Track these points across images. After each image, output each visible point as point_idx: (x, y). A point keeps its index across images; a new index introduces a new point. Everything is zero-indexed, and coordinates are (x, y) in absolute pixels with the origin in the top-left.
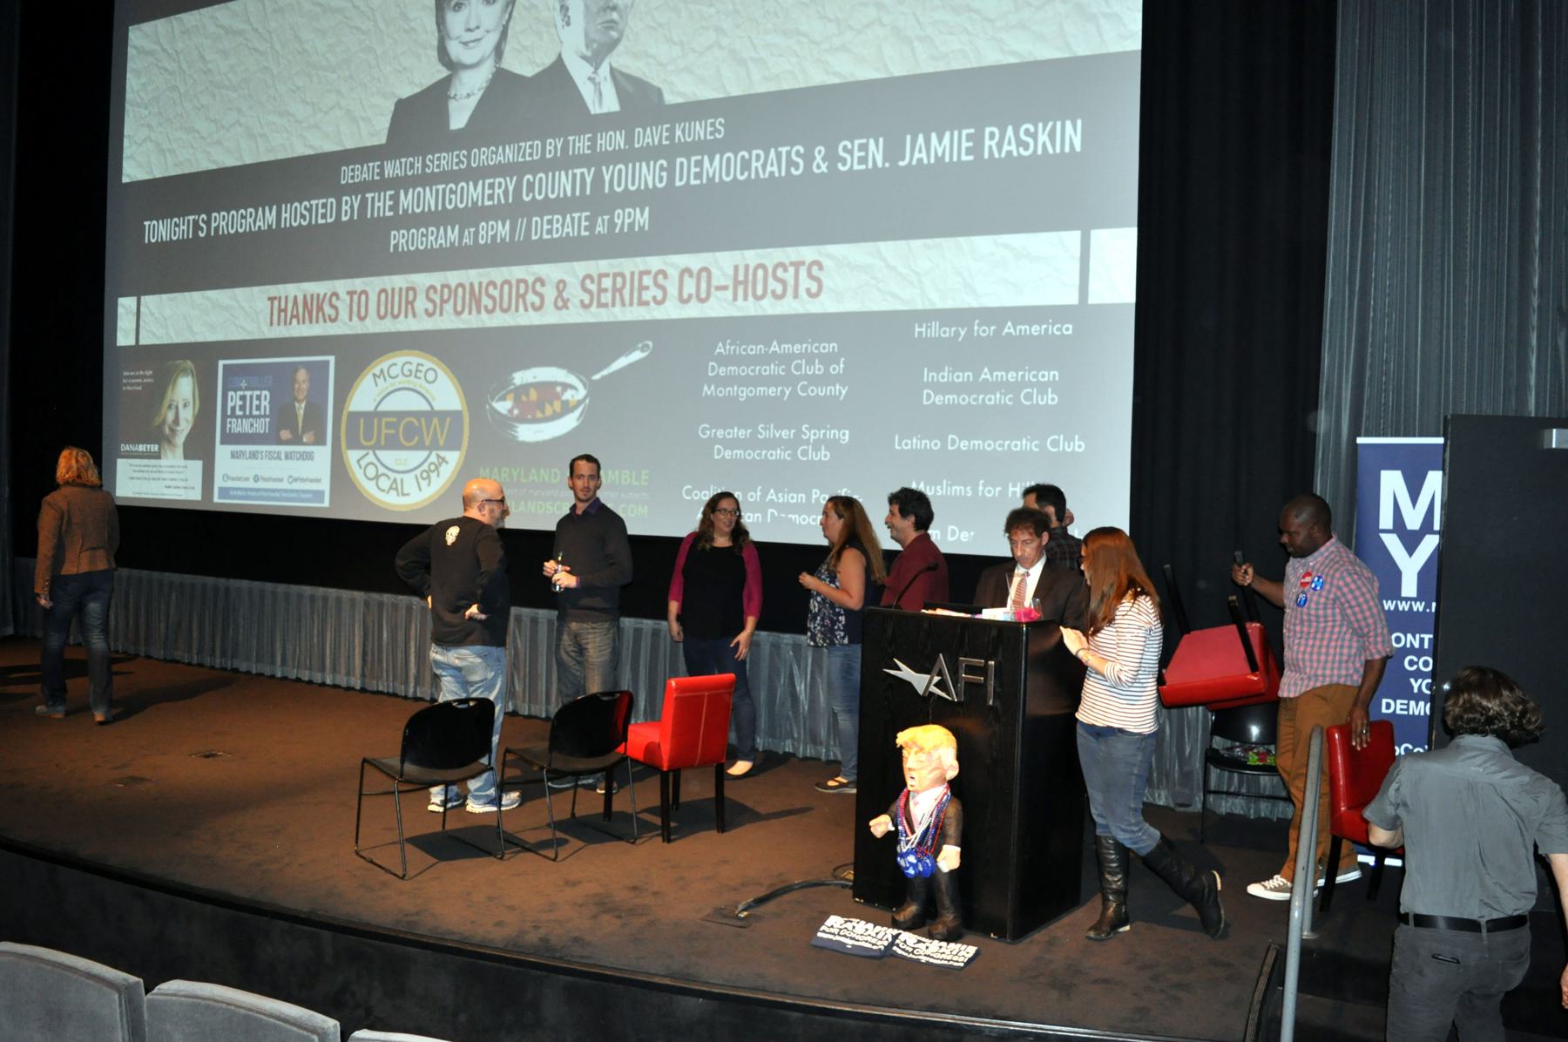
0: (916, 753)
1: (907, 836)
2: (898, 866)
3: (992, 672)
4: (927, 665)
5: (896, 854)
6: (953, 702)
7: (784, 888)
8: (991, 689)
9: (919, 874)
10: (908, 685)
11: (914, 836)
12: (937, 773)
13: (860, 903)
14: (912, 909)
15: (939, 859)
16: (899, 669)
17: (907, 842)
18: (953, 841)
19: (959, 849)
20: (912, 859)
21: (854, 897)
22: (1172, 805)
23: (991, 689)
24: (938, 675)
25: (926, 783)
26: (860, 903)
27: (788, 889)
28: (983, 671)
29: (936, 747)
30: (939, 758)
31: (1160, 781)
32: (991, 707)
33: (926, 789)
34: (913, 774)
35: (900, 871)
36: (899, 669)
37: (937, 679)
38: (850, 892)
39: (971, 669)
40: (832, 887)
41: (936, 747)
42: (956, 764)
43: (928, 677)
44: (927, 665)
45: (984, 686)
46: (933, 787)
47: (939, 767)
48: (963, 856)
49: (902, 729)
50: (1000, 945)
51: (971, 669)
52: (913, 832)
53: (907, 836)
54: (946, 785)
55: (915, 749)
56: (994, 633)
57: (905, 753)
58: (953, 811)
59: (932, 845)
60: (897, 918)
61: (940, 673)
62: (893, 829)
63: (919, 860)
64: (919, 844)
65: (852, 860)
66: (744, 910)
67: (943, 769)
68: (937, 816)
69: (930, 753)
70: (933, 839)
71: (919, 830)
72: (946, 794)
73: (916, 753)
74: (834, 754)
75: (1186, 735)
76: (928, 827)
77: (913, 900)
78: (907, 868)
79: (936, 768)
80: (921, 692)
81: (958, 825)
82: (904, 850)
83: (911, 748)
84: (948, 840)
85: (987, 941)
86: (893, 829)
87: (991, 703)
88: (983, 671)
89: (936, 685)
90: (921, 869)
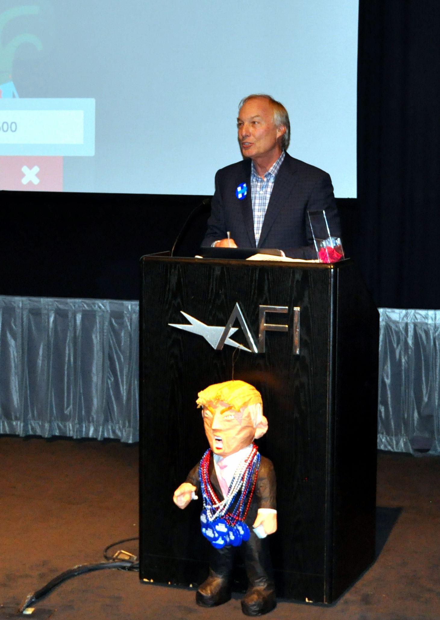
0: (222, 412)
1: (213, 503)
2: (205, 538)
3: (297, 319)
4: (221, 316)
5: (199, 525)
6: (253, 353)
7: (58, 578)
8: (297, 339)
9: (229, 545)
10: (200, 339)
11: (223, 503)
12: (244, 434)
13: (149, 583)
14: (218, 581)
15: (256, 525)
16: (188, 323)
17: (214, 511)
18: (268, 503)
19: (274, 512)
20: (221, 528)
21: (141, 577)
22: (411, 451)
23: (297, 339)
24: (234, 327)
25: (234, 445)
26: (149, 583)
27: (69, 575)
28: (288, 318)
29: (245, 405)
30: (249, 416)
31: (398, 426)
32: (298, 356)
33: (235, 451)
34: (220, 435)
35: (207, 542)
36: (188, 323)
37: (233, 330)
38: (136, 574)
39: (272, 317)
40: (107, 571)
41: (245, 405)
42: (264, 420)
43: (222, 329)
44: (221, 316)
45: (289, 335)
46: (242, 448)
47: (250, 426)
48: (280, 519)
49: (203, 388)
50: (316, 610)
51: (272, 317)
52: (221, 499)
53: (213, 503)
54: (252, 445)
55: (221, 408)
56: (298, 277)
57: (207, 414)
58: (264, 471)
59: (244, 512)
60: (203, 593)
61: (237, 324)
62: (196, 498)
63: (230, 529)
64: (229, 511)
65: (137, 535)
66: (29, 606)
67: (252, 427)
68: (249, 478)
69: (239, 411)
70: (245, 504)
71: (228, 499)
72: (255, 454)
73: (222, 412)
74: (33, 429)
75: (424, 379)
76: (239, 492)
77: (217, 570)
78: (216, 539)
79: (247, 427)
80: (215, 346)
81: (272, 486)
82: (211, 520)
83: (215, 407)
84: (263, 502)
85: (302, 606)
86: (196, 498)
87: (298, 352)
88: (288, 318)
89: (232, 337)
90: (232, 537)
